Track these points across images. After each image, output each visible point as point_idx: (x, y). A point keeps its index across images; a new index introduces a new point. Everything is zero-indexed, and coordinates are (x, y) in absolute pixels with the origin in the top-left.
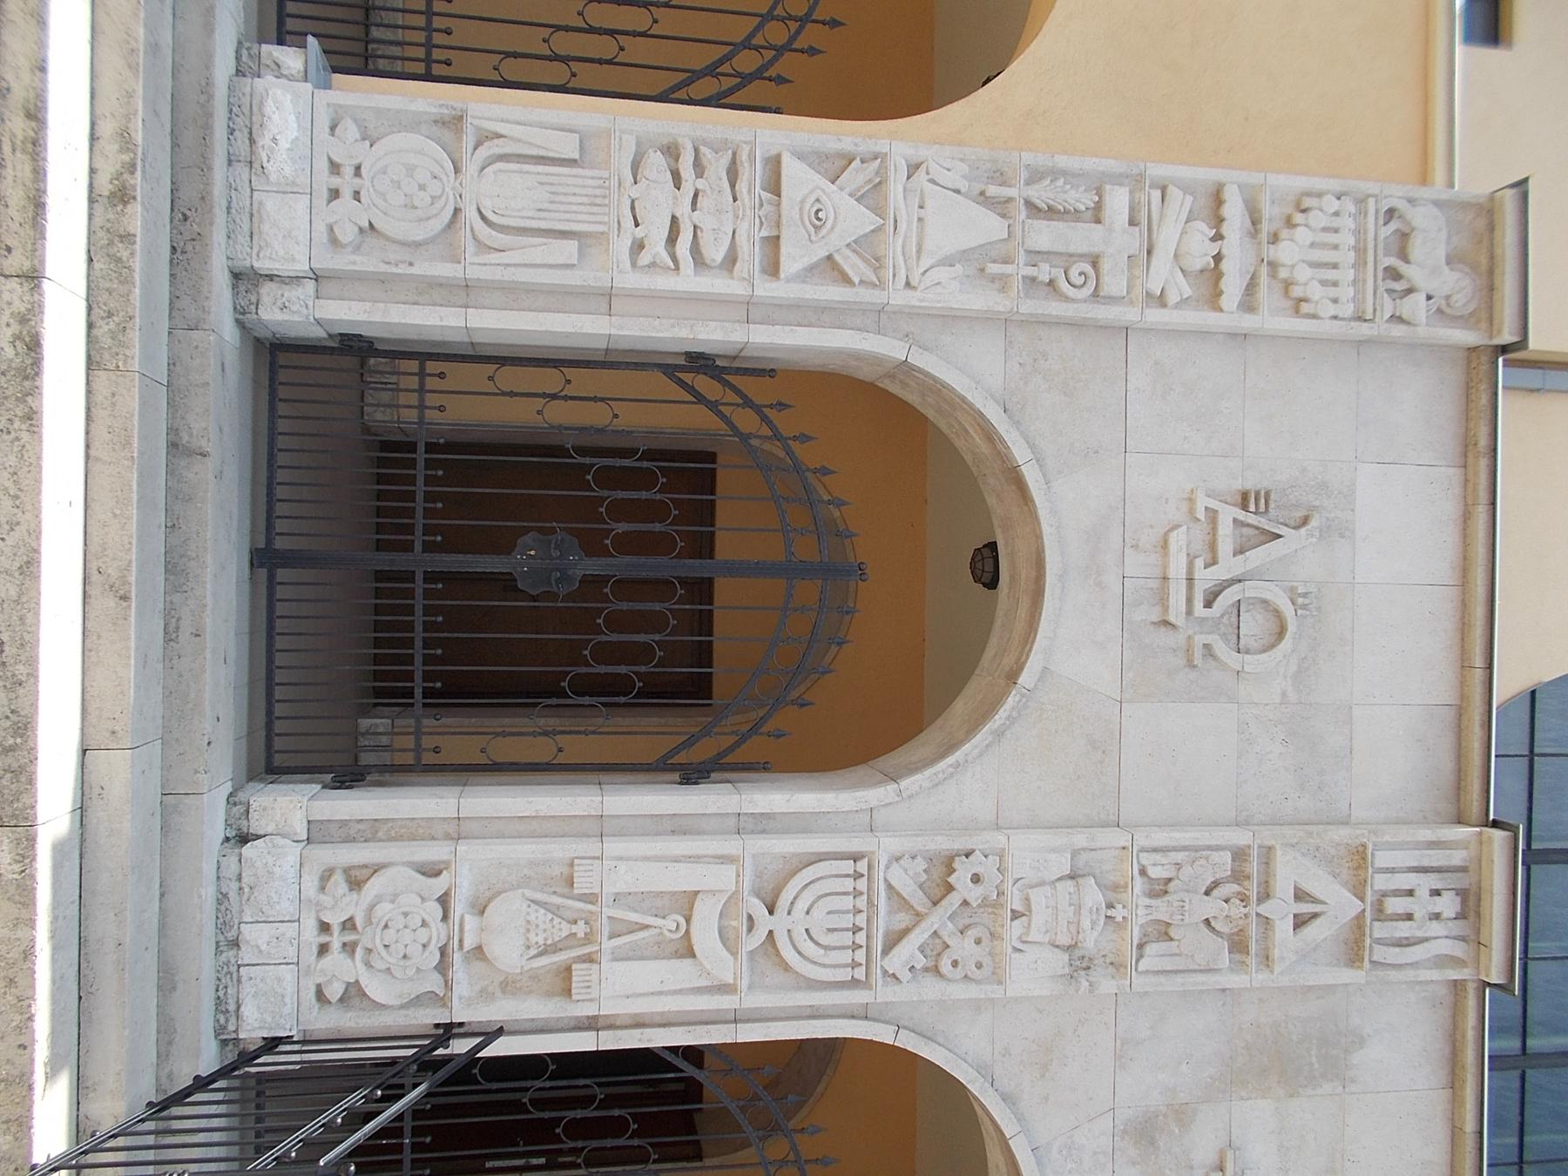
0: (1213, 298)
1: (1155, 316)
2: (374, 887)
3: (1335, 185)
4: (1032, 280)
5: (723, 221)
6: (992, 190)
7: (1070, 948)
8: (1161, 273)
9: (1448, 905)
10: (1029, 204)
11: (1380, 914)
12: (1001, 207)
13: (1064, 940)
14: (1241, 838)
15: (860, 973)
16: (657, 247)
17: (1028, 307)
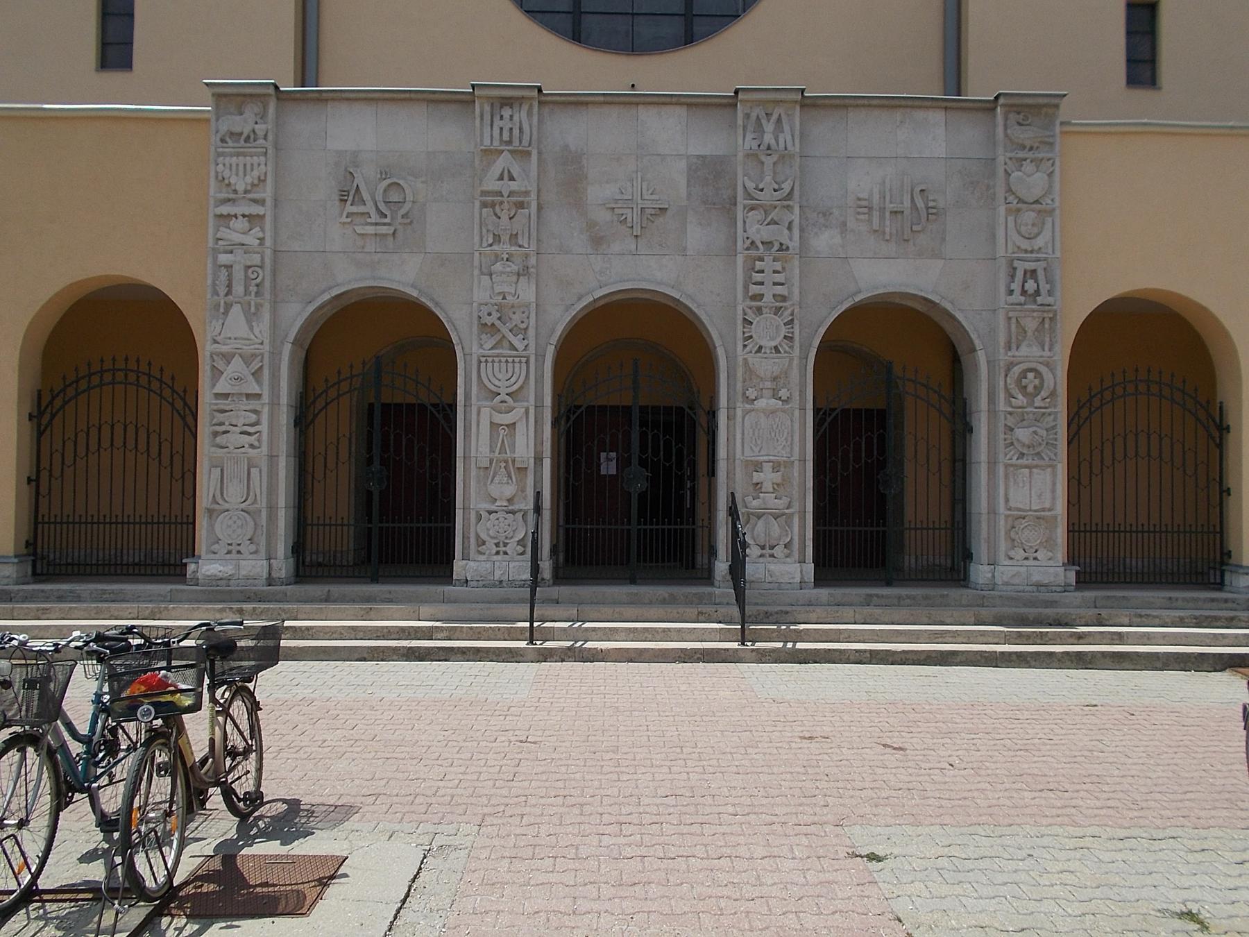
0: (262, 217)
1: (268, 242)
2: (484, 536)
3: (212, 167)
4: (257, 294)
5: (241, 414)
6: (222, 310)
7: (519, 275)
8: (251, 240)
9: (507, 112)
10: (227, 295)
11: (510, 142)
12: (228, 306)
13: (514, 278)
14: (477, 204)
15: (524, 360)
16: (252, 439)
17: (267, 296)
